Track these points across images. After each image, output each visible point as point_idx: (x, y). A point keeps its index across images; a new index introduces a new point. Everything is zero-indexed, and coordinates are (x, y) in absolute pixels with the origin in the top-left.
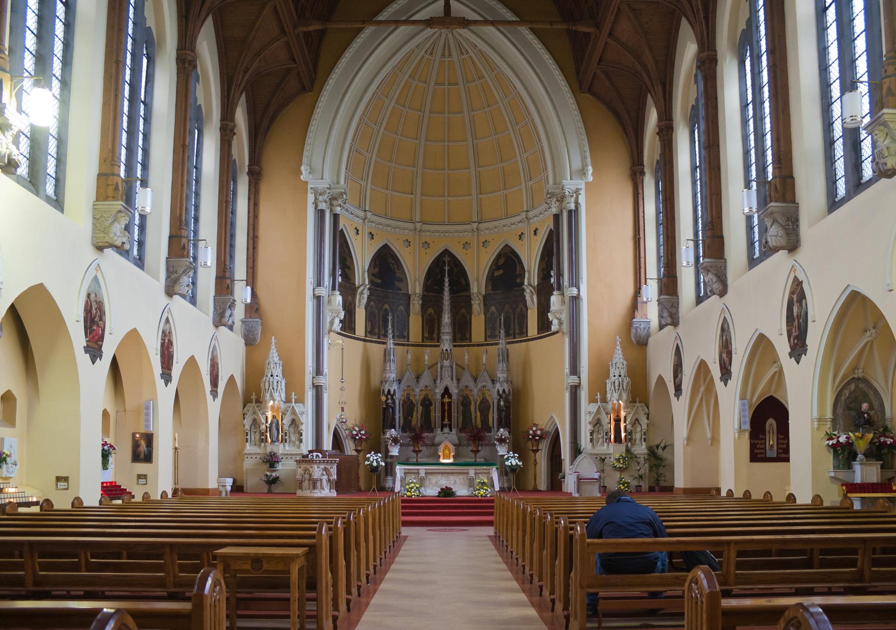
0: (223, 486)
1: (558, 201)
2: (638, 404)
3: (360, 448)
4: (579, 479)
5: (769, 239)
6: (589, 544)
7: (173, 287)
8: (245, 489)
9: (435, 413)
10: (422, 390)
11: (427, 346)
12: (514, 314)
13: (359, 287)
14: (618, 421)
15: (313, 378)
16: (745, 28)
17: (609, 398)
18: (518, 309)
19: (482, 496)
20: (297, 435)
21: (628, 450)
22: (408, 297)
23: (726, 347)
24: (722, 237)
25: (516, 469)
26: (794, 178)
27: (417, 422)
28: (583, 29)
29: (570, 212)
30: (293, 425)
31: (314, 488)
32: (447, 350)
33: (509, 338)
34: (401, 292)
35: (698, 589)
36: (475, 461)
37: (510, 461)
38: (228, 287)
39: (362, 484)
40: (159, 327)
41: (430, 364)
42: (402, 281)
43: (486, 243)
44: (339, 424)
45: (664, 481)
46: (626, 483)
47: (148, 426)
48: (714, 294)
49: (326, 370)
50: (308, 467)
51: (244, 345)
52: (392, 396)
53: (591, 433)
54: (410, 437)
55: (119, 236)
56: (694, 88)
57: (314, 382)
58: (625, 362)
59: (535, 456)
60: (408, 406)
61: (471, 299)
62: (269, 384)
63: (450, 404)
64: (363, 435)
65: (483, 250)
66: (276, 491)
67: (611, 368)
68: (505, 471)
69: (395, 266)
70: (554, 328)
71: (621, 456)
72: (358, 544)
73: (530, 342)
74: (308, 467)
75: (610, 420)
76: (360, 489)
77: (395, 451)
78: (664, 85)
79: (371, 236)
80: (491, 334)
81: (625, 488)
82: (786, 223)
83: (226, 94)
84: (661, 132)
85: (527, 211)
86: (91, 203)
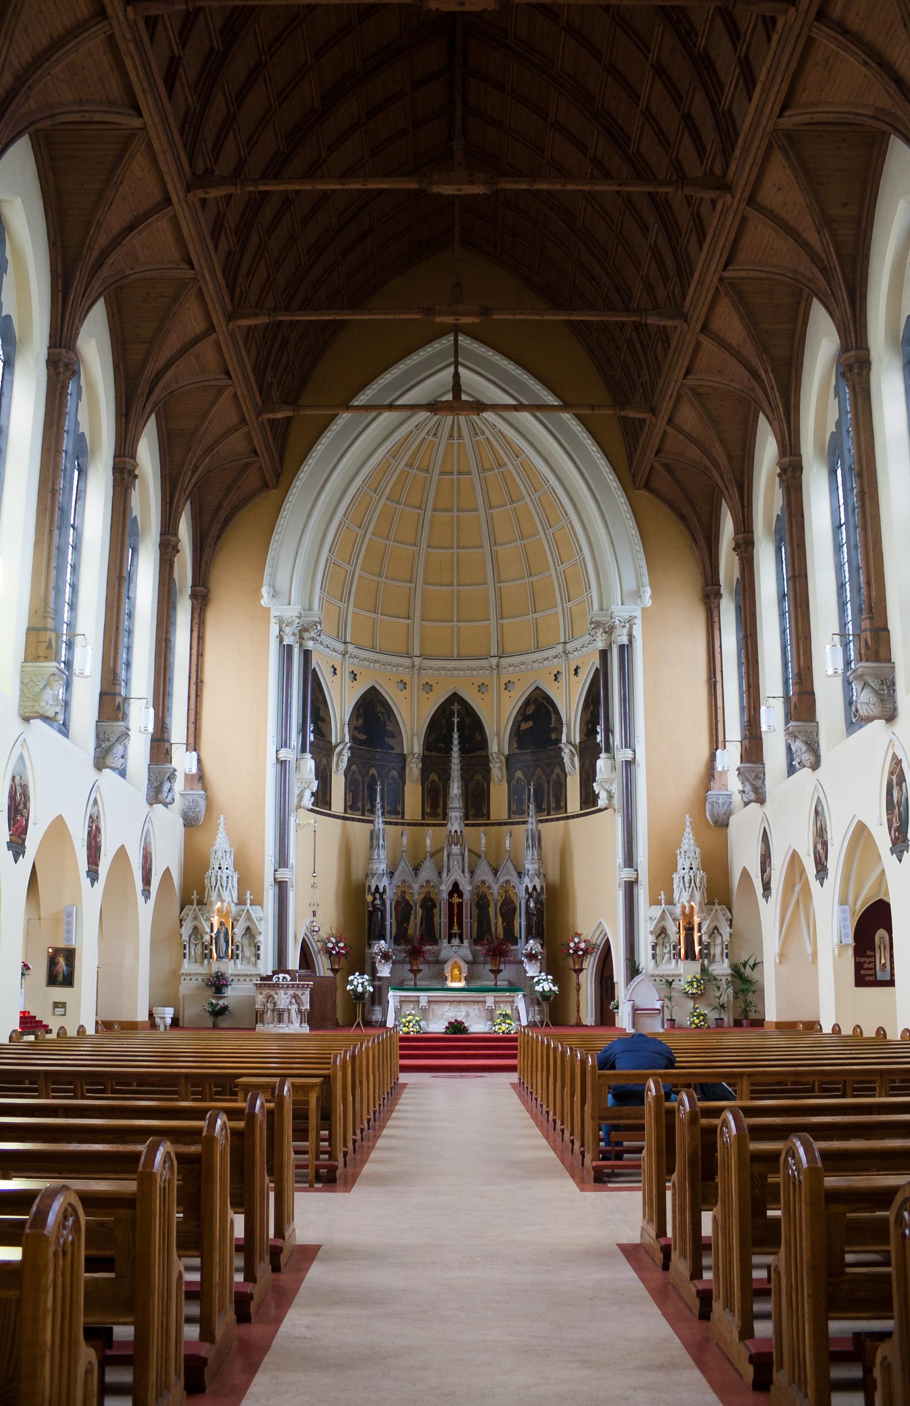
0: (161, 1018)
1: (606, 632)
2: (717, 907)
3: (337, 967)
4: (635, 1009)
5: (859, 707)
6: (600, 1076)
7: (104, 758)
8: (180, 1022)
9: (440, 918)
10: (422, 887)
11: (428, 825)
12: (548, 782)
13: (336, 746)
14: (689, 930)
15: (275, 871)
16: (835, 430)
17: (677, 899)
18: (554, 776)
19: (503, 1032)
20: (253, 949)
21: (704, 970)
22: (403, 757)
23: (821, 835)
24: (812, 694)
25: (549, 997)
26: (889, 631)
27: (416, 931)
28: (632, 415)
29: (622, 647)
30: (248, 936)
31: (280, 1021)
32: (456, 831)
33: (542, 814)
34: (394, 751)
35: (794, 1164)
36: (496, 985)
37: (541, 985)
38: (49, 646)
39: (340, 1017)
40: (86, 812)
41: (433, 851)
42: (395, 737)
43: (509, 685)
44: (309, 935)
45: (755, 1011)
46: (702, 1015)
47: (69, 939)
48: (804, 766)
49: (292, 860)
50: (272, 993)
51: (183, 826)
52: (381, 895)
53: (653, 946)
54: (405, 952)
55: (51, 705)
56: (833, 404)
57: (277, 876)
58: (698, 850)
59: (578, 978)
60: (403, 908)
61: (488, 761)
62: (217, 880)
63: (460, 905)
64: (342, 948)
65: (505, 694)
66: (224, 1026)
67: (679, 857)
68: (539, 1000)
69: (385, 716)
70: (602, 802)
71: (695, 977)
72: (361, 1083)
73: (571, 821)
74: (272, 993)
75: (679, 928)
76: (338, 1023)
77: (384, 971)
78: (740, 487)
79: (352, 675)
80: (517, 809)
81: (700, 1022)
82: (880, 687)
83: (168, 500)
84: (739, 548)
85: (565, 643)
86: (20, 665)
